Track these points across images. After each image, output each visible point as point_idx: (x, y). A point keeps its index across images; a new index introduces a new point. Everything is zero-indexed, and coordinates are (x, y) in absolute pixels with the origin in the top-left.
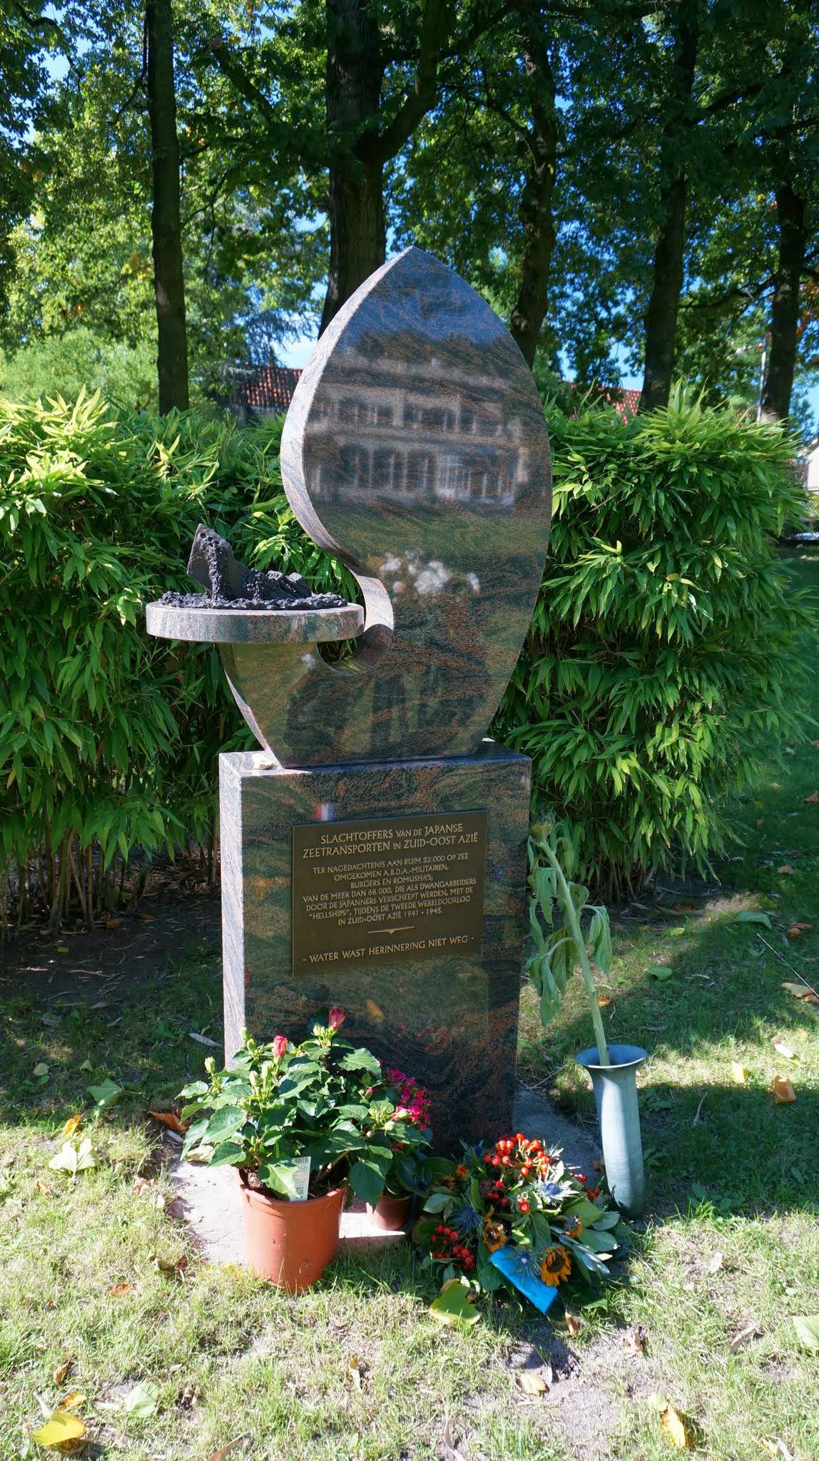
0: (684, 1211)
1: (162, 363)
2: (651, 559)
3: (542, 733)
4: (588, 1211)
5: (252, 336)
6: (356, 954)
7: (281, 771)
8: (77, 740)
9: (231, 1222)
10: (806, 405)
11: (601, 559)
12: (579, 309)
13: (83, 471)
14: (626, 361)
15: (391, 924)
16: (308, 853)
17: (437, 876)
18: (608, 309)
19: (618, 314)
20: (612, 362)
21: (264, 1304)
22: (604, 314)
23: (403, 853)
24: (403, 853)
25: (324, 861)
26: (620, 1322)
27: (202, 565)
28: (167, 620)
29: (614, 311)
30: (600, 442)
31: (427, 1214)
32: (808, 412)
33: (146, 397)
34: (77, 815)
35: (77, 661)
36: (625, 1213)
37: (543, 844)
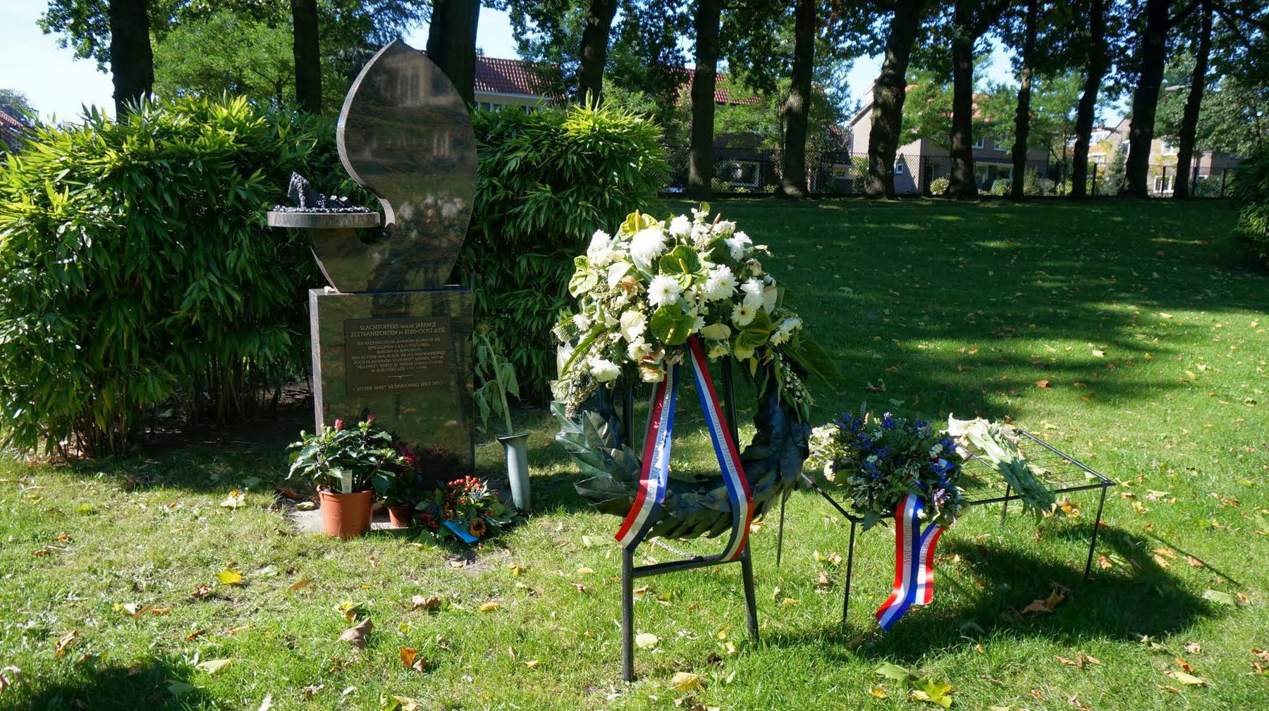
0: (550, 510)
1: (297, 48)
2: (572, 195)
3: (517, 297)
4: (497, 507)
5: (381, 22)
6: (381, 387)
7: (338, 293)
8: (237, 297)
9: (317, 520)
10: (846, 86)
11: (538, 193)
12: (650, 7)
13: (341, 428)
14: (690, 50)
15: (401, 373)
16: (353, 335)
17: (424, 349)
18: (673, 9)
19: (682, 14)
20: (679, 51)
21: (332, 544)
22: (670, 13)
23: (405, 337)
24: (405, 337)
25: (362, 339)
26: (504, 547)
27: (295, 191)
28: (278, 217)
29: (679, 10)
30: (543, 128)
31: (418, 512)
32: (847, 92)
33: (286, 74)
34: (236, 343)
35: (235, 252)
36: (519, 511)
37: (483, 336)
